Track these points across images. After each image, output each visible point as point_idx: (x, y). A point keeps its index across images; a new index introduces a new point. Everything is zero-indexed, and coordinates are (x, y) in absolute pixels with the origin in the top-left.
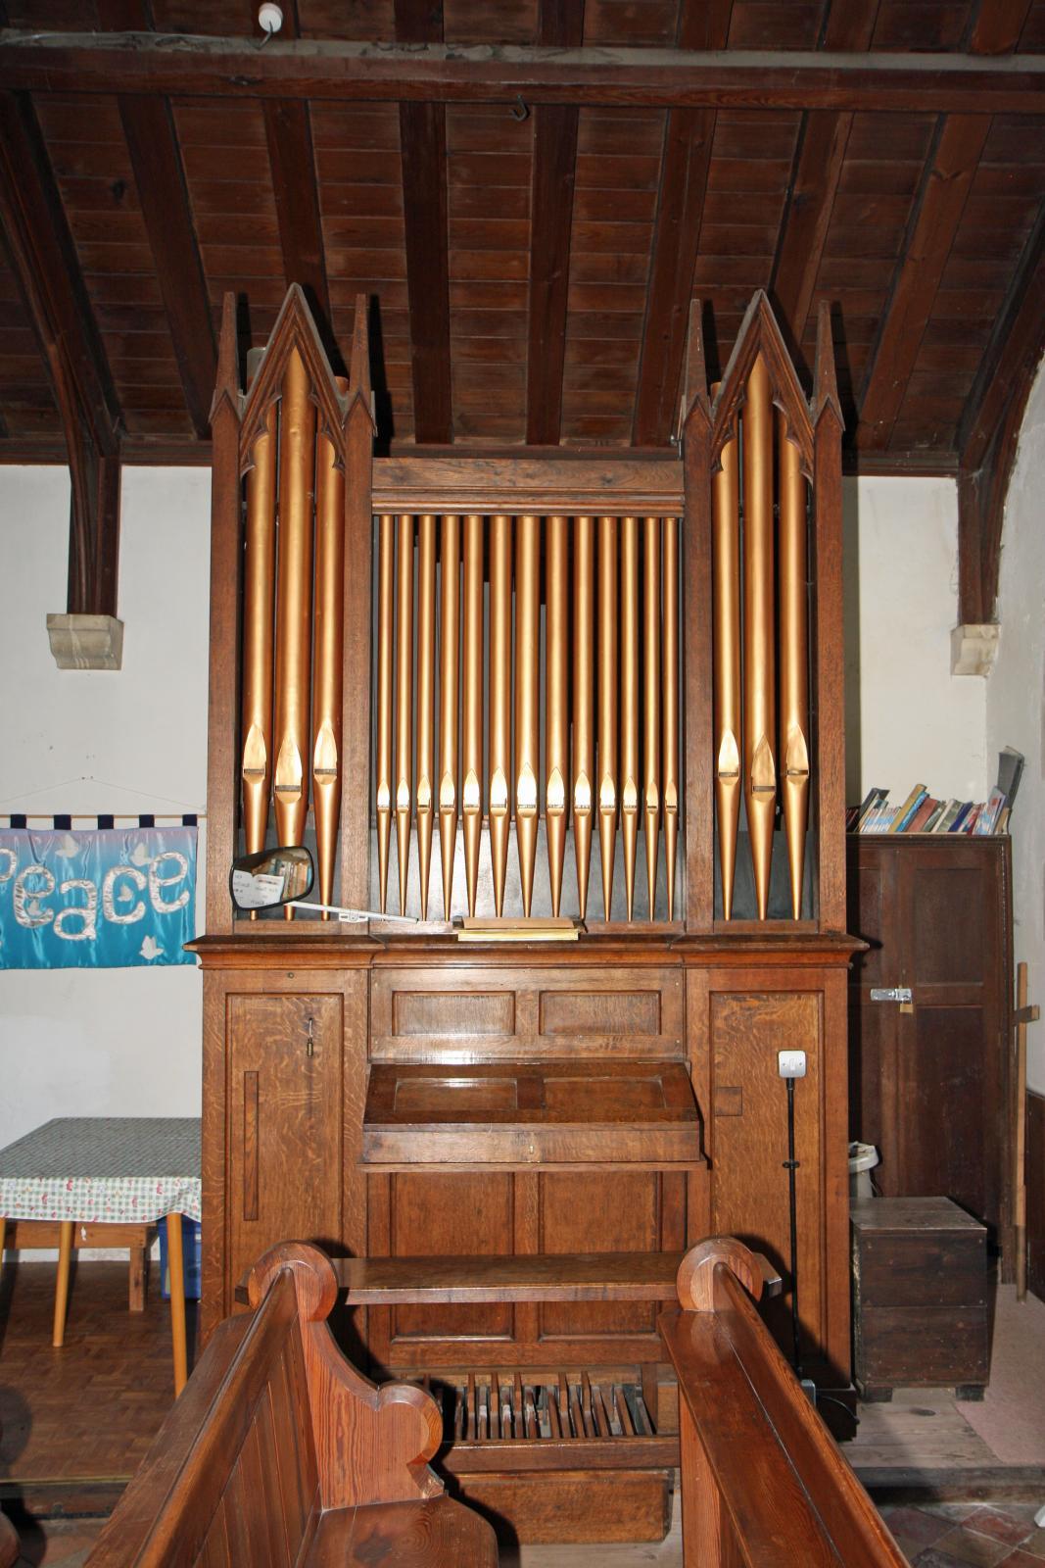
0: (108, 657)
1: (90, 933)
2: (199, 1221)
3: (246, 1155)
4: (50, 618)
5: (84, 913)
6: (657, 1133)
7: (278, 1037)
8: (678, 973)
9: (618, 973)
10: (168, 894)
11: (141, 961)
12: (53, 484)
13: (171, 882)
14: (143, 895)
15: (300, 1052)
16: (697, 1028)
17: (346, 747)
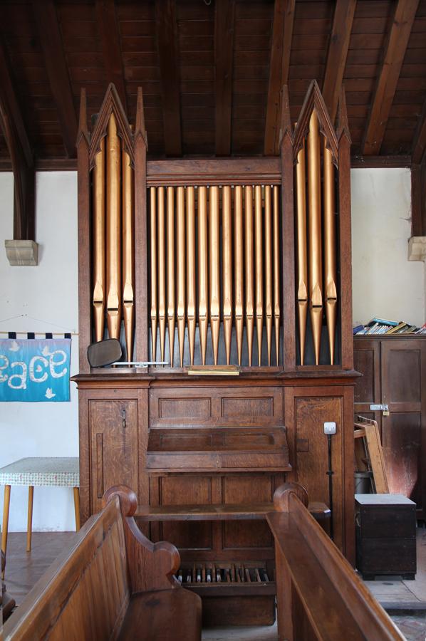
0: (34, 258)
1: (24, 386)
2: (111, 85)
3: (98, 470)
4: (7, 242)
5: (21, 376)
6: (271, 455)
7: (110, 419)
8: (281, 389)
9: (255, 389)
10: (58, 370)
13: (59, 364)
14: (47, 370)
15: (120, 425)
16: (289, 413)
17: (137, 290)
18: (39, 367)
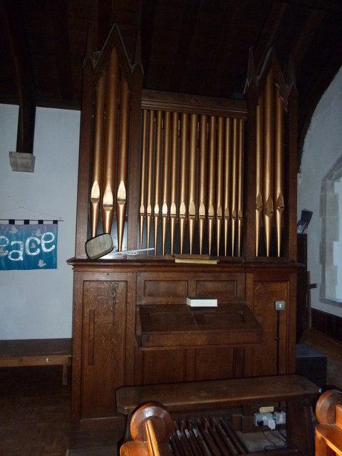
0: (29, 168)
1: (21, 258)
4: (11, 153)
10: (48, 246)
11: (39, 268)
12: (12, 111)
13: (48, 242)
14: (40, 246)
18: (33, 244)
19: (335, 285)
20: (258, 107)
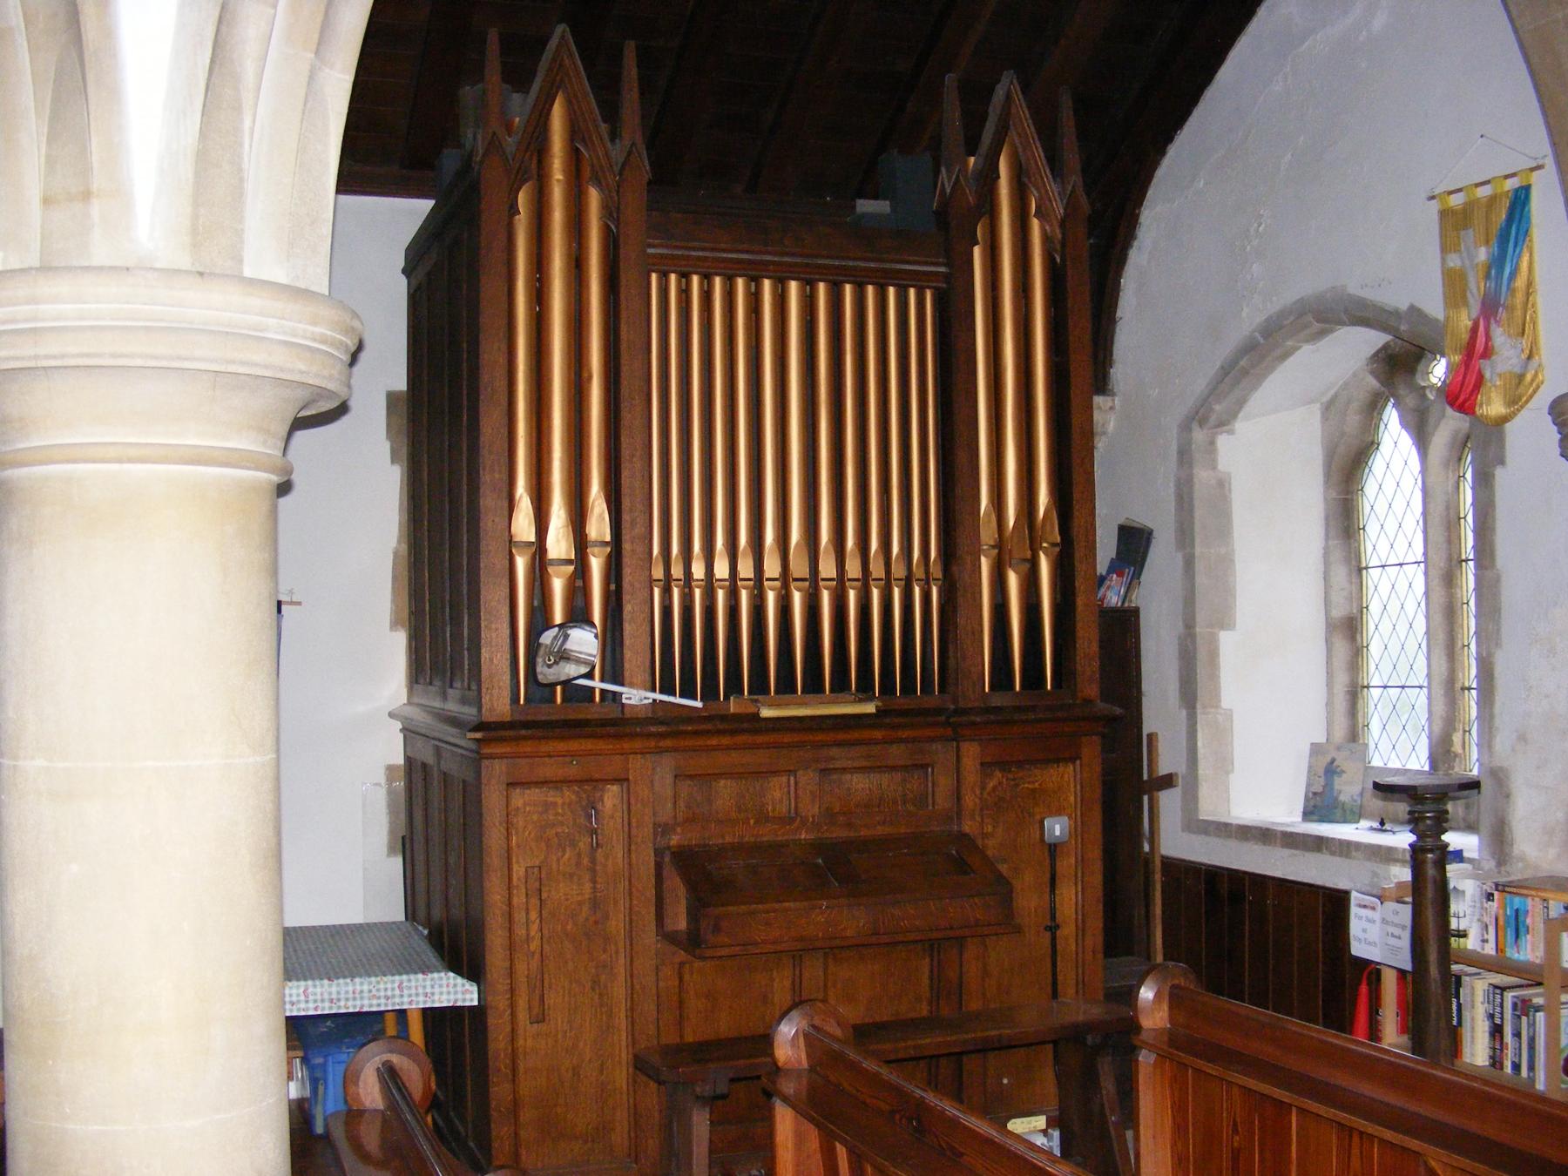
19: (1227, 773)
20: (977, 251)
